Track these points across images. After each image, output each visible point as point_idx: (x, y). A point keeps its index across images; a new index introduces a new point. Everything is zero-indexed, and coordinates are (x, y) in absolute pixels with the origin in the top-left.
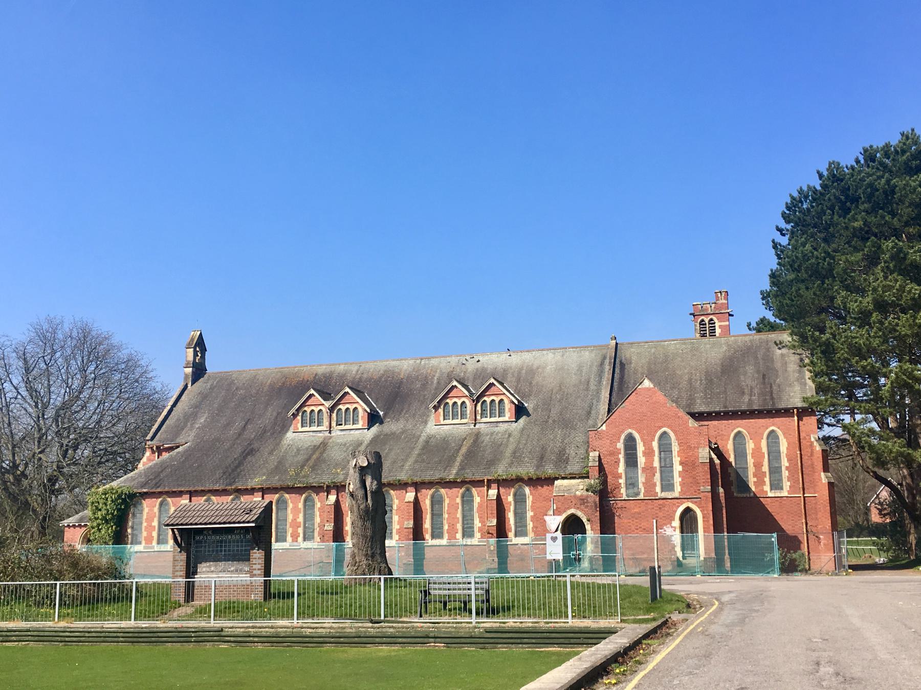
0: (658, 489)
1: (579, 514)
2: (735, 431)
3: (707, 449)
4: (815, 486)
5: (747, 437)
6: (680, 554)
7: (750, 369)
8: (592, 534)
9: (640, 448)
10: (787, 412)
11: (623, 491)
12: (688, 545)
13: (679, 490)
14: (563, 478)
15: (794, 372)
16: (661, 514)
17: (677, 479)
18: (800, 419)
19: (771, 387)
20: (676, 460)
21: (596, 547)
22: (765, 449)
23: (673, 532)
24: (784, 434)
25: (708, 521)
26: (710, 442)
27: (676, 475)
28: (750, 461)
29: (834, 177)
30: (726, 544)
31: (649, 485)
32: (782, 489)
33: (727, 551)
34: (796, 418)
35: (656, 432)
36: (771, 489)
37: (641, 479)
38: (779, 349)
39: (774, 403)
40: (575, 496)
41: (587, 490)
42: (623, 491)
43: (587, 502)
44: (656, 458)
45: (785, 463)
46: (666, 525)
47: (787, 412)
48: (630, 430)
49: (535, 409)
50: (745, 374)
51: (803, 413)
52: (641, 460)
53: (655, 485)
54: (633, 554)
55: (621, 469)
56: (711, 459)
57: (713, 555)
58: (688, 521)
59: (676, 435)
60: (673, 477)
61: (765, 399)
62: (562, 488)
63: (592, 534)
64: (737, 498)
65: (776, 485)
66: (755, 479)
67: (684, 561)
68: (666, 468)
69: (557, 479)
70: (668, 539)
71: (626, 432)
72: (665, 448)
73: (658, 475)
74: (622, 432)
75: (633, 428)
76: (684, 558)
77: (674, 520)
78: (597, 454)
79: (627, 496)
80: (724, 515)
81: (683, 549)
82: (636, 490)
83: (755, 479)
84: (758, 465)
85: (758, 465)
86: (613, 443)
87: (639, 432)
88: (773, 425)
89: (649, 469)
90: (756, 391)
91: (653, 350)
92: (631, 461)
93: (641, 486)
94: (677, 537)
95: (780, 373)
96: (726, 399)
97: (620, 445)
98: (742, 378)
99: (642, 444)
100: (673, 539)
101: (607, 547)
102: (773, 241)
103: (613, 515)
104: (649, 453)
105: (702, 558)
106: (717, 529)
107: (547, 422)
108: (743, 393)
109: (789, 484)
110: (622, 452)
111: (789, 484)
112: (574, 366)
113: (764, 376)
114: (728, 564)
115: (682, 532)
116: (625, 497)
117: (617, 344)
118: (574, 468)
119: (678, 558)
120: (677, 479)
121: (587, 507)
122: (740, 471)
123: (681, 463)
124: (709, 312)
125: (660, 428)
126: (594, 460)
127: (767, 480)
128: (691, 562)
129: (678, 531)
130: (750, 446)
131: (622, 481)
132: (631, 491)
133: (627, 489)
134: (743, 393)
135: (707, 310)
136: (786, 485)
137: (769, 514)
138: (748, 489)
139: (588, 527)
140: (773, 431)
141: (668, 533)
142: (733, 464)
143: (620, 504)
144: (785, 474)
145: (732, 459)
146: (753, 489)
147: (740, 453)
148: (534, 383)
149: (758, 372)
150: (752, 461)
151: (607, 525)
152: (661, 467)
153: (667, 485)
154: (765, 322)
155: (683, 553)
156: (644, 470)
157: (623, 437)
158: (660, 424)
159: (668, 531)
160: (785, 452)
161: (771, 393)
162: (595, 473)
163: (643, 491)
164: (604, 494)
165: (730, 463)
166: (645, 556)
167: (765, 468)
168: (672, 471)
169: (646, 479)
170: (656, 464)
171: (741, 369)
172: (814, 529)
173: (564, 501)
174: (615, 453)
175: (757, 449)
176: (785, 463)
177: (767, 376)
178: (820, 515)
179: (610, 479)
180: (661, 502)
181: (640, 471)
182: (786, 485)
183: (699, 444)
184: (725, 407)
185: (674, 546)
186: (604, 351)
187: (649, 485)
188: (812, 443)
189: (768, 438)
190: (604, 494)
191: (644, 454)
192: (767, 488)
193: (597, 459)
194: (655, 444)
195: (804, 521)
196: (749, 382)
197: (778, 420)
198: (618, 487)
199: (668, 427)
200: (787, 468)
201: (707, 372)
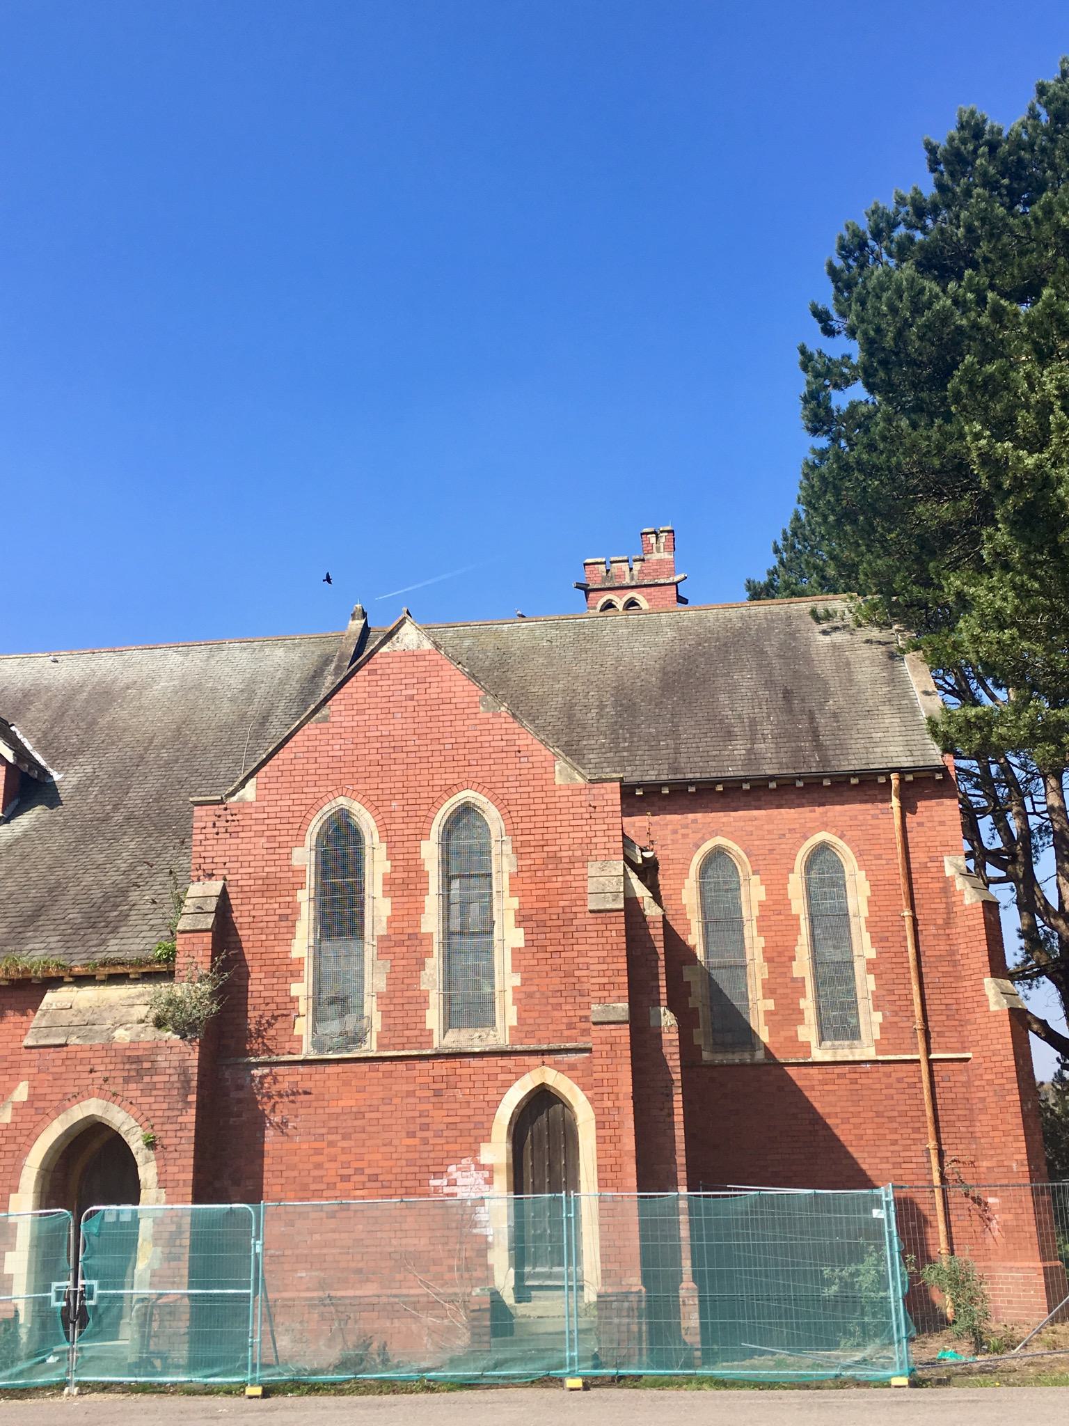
0: (433, 1018)
1: (120, 1119)
2: (707, 846)
3: (618, 866)
4: (964, 1023)
5: (744, 866)
6: (504, 1279)
7: (746, 680)
8: (160, 1206)
9: (377, 865)
10: (868, 785)
11: (303, 1027)
12: (540, 1244)
13: (512, 1020)
14: (81, 980)
15: (874, 682)
16: (439, 1118)
17: (506, 980)
18: (908, 807)
19: (812, 719)
20: (505, 907)
21: (170, 1258)
22: (799, 906)
23: (482, 1187)
24: (859, 855)
25: (615, 1140)
26: (627, 842)
27: (502, 962)
28: (754, 943)
29: (966, 155)
30: (684, 1232)
31: (403, 1003)
32: (854, 1034)
33: (687, 1266)
34: (895, 802)
35: (434, 805)
36: (822, 1039)
37: (374, 979)
38: (825, 632)
39: (824, 760)
40: (109, 1047)
41: (159, 1023)
42: (303, 1027)
43: (153, 1071)
44: (432, 903)
45: (864, 948)
46: (456, 1158)
47: (868, 785)
48: (342, 801)
49: (80, 789)
50: (732, 690)
51: (920, 785)
52: (378, 909)
53: (423, 1001)
54: (322, 1285)
55: (302, 943)
56: (632, 904)
57: (634, 1282)
58: (541, 1138)
59: (507, 813)
60: (489, 973)
61: (800, 749)
62: (65, 1018)
63: (160, 1206)
64: (712, 1066)
65: (838, 1023)
66: (770, 1004)
67: (522, 1309)
68: (468, 936)
69: (55, 982)
70: (461, 1220)
71: (328, 809)
72: (465, 864)
73: (434, 967)
74: (314, 807)
75: (354, 794)
76: (522, 1293)
77: (487, 1138)
78: (215, 887)
79: (319, 1045)
80: (679, 1118)
81: (520, 1256)
82: (350, 1023)
83: (770, 1004)
84: (779, 957)
85: (779, 957)
86: (280, 849)
87: (375, 808)
88: (825, 826)
89: (404, 944)
90: (767, 729)
91: (467, 643)
92: (341, 913)
93: (371, 1007)
94: (496, 1211)
95: (833, 685)
96: (677, 751)
97: (304, 857)
98: (723, 699)
99: (368, 816)
100: (482, 1215)
101: (213, 1257)
102: (803, 351)
103: (259, 1122)
104: (405, 884)
105: (590, 1296)
106: (652, 1174)
107: (107, 818)
108: (729, 735)
109: (878, 1017)
110: (310, 880)
111: (878, 1017)
112: (236, 682)
113: (787, 695)
114: (691, 1320)
115: (518, 1186)
116: (307, 1051)
117: (366, 630)
118: (133, 943)
119: (496, 1299)
120: (506, 980)
121: (149, 1090)
122: (720, 977)
123: (522, 919)
124: (627, 581)
125: (449, 791)
126: (200, 911)
127: (808, 1004)
128: (547, 1311)
129: (502, 1182)
130: (753, 894)
131: (301, 989)
132: (333, 1027)
133: (317, 1018)
134: (729, 735)
135: (621, 576)
136: (871, 1021)
137: (817, 1121)
138: (747, 1037)
139: (147, 1172)
140: (823, 848)
141: (462, 1193)
142: (700, 954)
143: (288, 1078)
144: (865, 984)
145: (695, 939)
146: (764, 1036)
147: (722, 917)
148: (103, 722)
149: (769, 684)
150: (761, 942)
151: (226, 1159)
152: (448, 934)
153: (468, 1007)
154: (880, 212)
155: (520, 1277)
156: (387, 945)
157: (315, 826)
158: (451, 778)
159: (464, 1183)
160: (864, 912)
161: (815, 734)
162: (196, 957)
163: (377, 1025)
164: (226, 1037)
165: (690, 954)
166: (370, 1289)
167: (802, 967)
168: (489, 951)
169: (391, 981)
170: (431, 923)
171: (720, 681)
172: (966, 1173)
173: (64, 1064)
174: (277, 886)
175: (776, 907)
176: (864, 948)
177: (795, 693)
178: (983, 1123)
179: (257, 984)
180: (441, 1068)
181: (370, 952)
182: (871, 1021)
183: (589, 845)
184: (676, 770)
185: (484, 1248)
186: (329, 648)
187: (403, 1003)
188: (947, 884)
189: (808, 868)
190: (226, 1037)
191: (390, 885)
192: (808, 1032)
193: (212, 905)
194: (430, 851)
195: (932, 1144)
196: (744, 708)
197: (836, 811)
198: (284, 1012)
199: (480, 786)
200: (872, 966)
201: (619, 690)
